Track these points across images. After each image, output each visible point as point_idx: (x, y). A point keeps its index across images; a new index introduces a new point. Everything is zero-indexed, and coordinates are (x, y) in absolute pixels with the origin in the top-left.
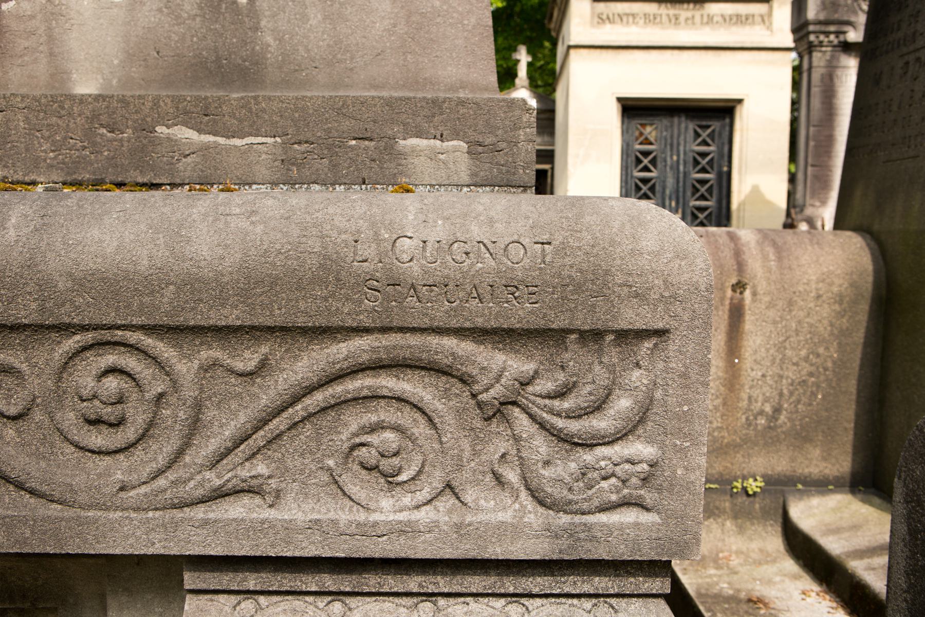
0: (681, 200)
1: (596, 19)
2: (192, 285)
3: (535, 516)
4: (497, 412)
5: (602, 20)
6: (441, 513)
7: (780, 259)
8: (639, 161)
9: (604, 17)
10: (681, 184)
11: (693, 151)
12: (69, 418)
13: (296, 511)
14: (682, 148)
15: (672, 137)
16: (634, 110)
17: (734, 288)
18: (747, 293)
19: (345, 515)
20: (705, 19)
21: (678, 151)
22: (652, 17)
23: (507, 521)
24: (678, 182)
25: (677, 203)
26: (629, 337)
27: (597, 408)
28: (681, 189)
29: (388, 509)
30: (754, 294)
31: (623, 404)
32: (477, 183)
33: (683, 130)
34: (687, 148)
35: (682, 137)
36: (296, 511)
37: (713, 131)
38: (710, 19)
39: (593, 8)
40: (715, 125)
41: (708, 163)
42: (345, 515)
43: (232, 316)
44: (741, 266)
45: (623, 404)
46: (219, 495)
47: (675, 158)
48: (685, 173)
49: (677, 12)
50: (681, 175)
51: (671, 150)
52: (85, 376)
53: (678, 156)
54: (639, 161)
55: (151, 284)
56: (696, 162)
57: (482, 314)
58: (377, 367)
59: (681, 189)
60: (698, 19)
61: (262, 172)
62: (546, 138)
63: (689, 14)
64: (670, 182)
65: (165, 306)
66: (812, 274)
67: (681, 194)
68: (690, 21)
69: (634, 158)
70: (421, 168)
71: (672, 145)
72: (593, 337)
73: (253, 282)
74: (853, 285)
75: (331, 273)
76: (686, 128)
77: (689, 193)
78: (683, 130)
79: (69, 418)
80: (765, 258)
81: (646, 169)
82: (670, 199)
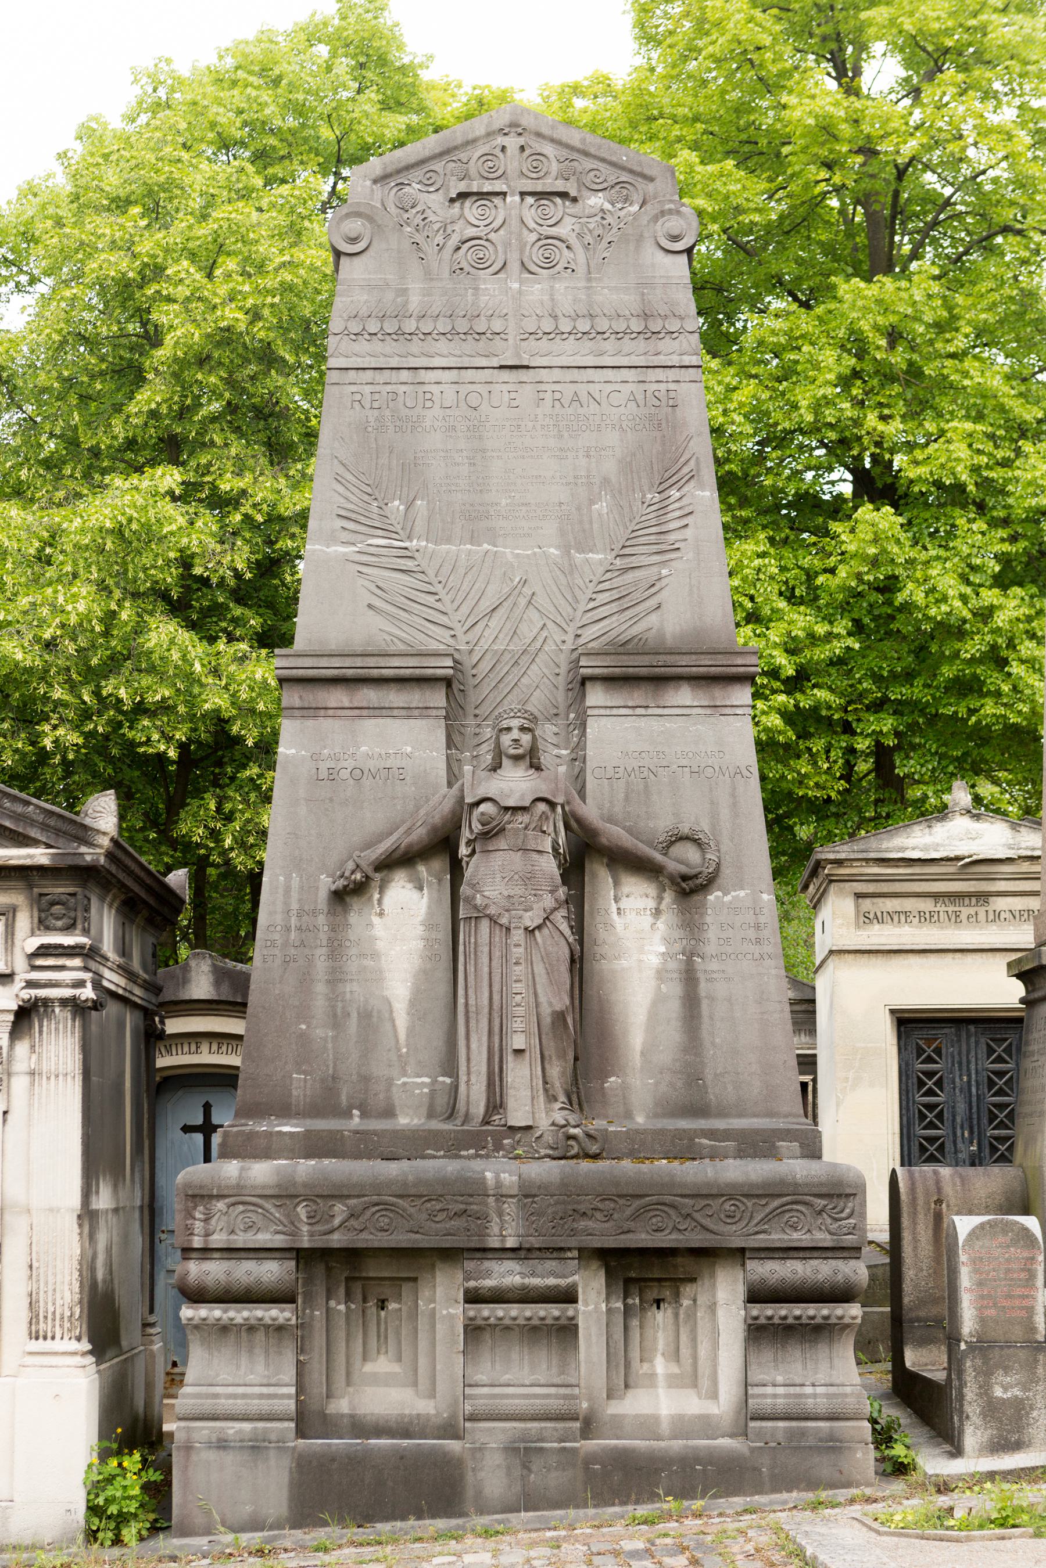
0: (976, 1129)
1: (862, 919)
2: (752, 1185)
3: (829, 1237)
4: (820, 1213)
5: (867, 919)
6: (808, 1236)
7: (963, 1185)
8: (921, 1084)
9: (871, 916)
10: (974, 1110)
11: (987, 1070)
12: (722, 1216)
13: (774, 1236)
14: (973, 1067)
15: (960, 1054)
16: (909, 1024)
17: (936, 1203)
18: (944, 1205)
19: (786, 1237)
20: (991, 917)
21: (969, 1070)
22: (927, 916)
23: (822, 1238)
24: (970, 1109)
25: (971, 1133)
26: (848, 1196)
27: (842, 1211)
28: (975, 1116)
29: (795, 1235)
30: (948, 1206)
31: (847, 1211)
32: (803, 1157)
33: (973, 1045)
34: (980, 1067)
35: (973, 1053)
36: (774, 1236)
37: (1011, 1044)
38: (997, 915)
39: (857, 906)
40: (1012, 1038)
41: (1005, 1083)
42: (786, 1237)
43: (760, 1192)
44: (939, 1190)
45: (847, 1211)
46: (757, 1233)
47: (965, 1078)
48: (978, 1096)
49: (957, 909)
50: (974, 1099)
51: (960, 1070)
52: (727, 1206)
53: (969, 1076)
54: (921, 1084)
55: (742, 1185)
56: (991, 1084)
57: (815, 1191)
58: (792, 1203)
59: (975, 1116)
60: (982, 916)
61: (731, 1154)
62: (804, 1039)
63: (972, 911)
64: (961, 1107)
65: (746, 1191)
66: (983, 1193)
67: (975, 1122)
68: (973, 918)
69: (915, 1080)
70: (784, 1151)
71: (960, 1063)
72: (839, 1196)
73: (766, 1184)
74: (1007, 1199)
75: (782, 1182)
76: (977, 1043)
77: (985, 1121)
78: (973, 1045)
79: (722, 1216)
80: (954, 1185)
81: (930, 1093)
82: (962, 1127)
